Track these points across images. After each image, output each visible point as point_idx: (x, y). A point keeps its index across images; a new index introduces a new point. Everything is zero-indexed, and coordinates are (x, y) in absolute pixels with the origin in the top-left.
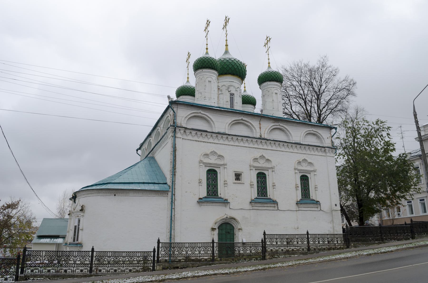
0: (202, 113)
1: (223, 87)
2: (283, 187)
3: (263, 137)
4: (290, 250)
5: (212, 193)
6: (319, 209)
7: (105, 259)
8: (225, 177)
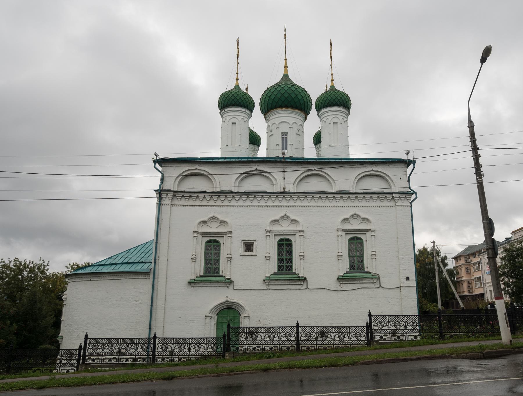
0: (200, 168)
1: (274, 125)
2: (321, 256)
3: (286, 190)
4: (283, 348)
5: (212, 272)
6: (378, 286)
7: (312, 336)
8: (231, 248)
